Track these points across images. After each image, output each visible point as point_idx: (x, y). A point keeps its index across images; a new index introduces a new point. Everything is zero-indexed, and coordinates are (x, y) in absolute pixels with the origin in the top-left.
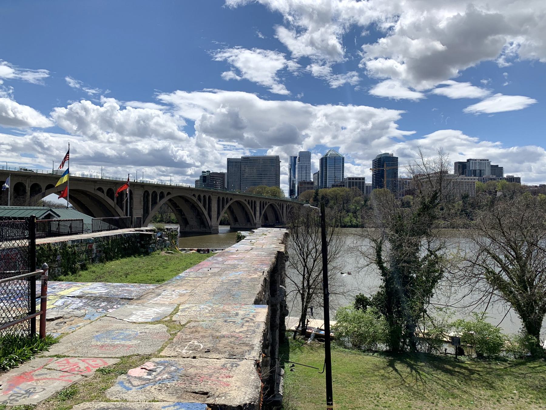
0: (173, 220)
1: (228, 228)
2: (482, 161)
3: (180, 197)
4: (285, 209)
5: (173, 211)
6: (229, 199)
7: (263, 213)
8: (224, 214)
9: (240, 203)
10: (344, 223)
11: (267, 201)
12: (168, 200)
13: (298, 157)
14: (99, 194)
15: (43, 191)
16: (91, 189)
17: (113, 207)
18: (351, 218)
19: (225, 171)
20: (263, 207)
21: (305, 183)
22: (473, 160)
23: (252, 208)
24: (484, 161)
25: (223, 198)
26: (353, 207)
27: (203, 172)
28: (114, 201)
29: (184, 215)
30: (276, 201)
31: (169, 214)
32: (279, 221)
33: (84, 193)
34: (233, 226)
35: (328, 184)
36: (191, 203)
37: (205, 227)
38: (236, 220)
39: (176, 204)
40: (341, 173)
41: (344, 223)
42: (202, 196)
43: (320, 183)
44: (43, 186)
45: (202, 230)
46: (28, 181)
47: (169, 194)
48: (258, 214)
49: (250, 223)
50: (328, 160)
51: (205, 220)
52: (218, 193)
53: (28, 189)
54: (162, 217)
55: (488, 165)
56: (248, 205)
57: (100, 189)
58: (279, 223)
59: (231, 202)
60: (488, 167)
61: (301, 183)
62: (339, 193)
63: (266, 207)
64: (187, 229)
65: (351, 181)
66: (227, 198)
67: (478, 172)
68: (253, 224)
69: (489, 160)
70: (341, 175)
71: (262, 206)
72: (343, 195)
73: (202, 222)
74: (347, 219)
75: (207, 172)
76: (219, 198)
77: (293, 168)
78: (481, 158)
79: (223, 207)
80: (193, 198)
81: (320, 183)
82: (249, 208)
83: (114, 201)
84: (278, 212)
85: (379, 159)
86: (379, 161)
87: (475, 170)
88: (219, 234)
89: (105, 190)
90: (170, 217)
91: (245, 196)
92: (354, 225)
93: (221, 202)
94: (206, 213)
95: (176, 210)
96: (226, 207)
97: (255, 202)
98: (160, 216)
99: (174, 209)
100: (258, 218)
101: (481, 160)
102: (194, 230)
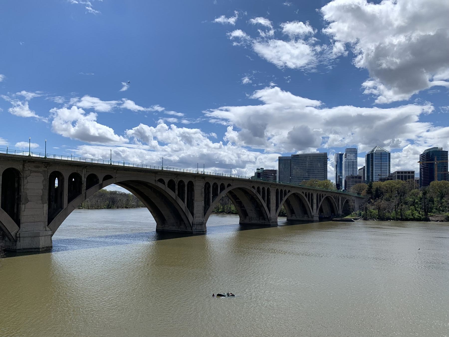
0: (233, 211)
1: (284, 220)
3: (239, 188)
4: (340, 201)
5: (233, 203)
6: (287, 191)
7: (319, 206)
8: (282, 207)
9: (297, 196)
10: (405, 216)
11: (324, 193)
12: (228, 192)
13: (345, 154)
14: (160, 185)
15: (101, 182)
16: (151, 180)
17: (175, 198)
18: (413, 211)
19: (277, 168)
20: (320, 200)
21: (353, 177)
23: (309, 200)
25: (281, 190)
26: (411, 200)
28: (175, 193)
31: (229, 205)
32: (334, 214)
33: (145, 184)
34: (290, 218)
37: (264, 219)
38: (292, 212)
39: (236, 196)
41: (405, 216)
42: (261, 188)
43: (366, 178)
44: (101, 177)
45: (261, 222)
46: (84, 171)
47: (229, 185)
48: (315, 207)
51: (264, 212)
52: (277, 185)
53: (84, 180)
54: (223, 208)
57: (161, 181)
58: (334, 215)
59: (289, 194)
62: (394, 186)
63: (322, 200)
64: (247, 221)
65: (404, 174)
66: (285, 191)
68: (310, 217)
71: (319, 199)
72: (399, 188)
73: (261, 214)
74: (408, 212)
75: (261, 169)
76: (277, 190)
77: (339, 164)
79: (281, 199)
80: (253, 190)
82: (307, 200)
83: (175, 192)
84: (334, 205)
85: (427, 153)
88: (278, 227)
89: (166, 181)
90: (230, 208)
91: (303, 188)
92: (417, 218)
93: (280, 194)
94: (265, 205)
95: (236, 202)
96: (285, 199)
97: (312, 194)
98: (222, 207)
99: (234, 201)
100: (315, 211)
102: (253, 222)
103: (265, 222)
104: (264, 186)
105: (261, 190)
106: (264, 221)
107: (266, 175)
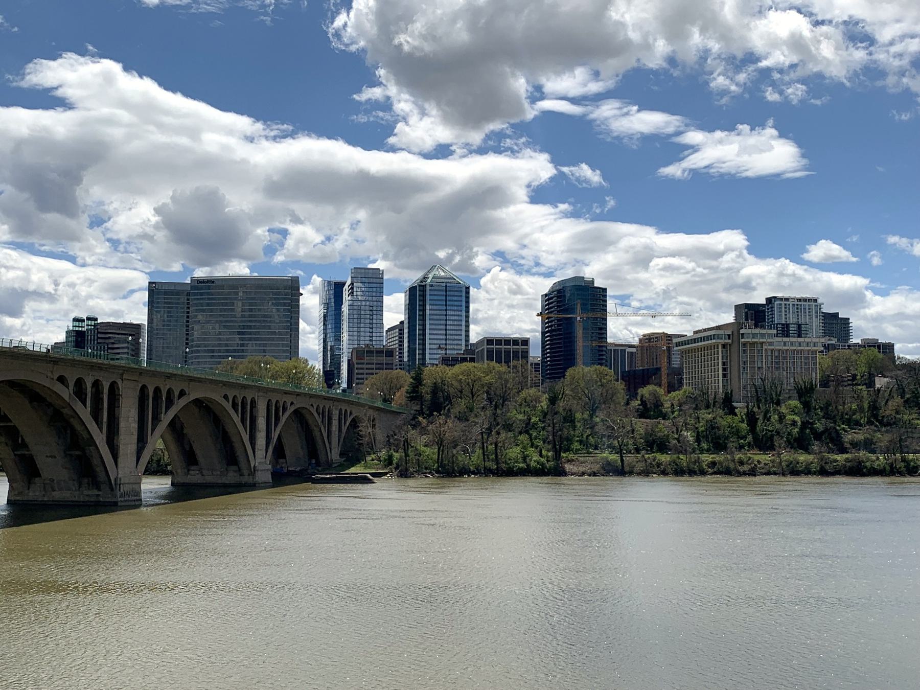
2: (802, 303)
4: (335, 423)
6: (177, 393)
7: (275, 436)
8: (157, 443)
18: (524, 447)
19: (138, 315)
21: (370, 352)
22: (781, 299)
23: (243, 421)
24: (807, 303)
25: (157, 390)
26: (520, 417)
27: (75, 320)
29: (24, 445)
30: (313, 400)
32: (317, 458)
34: (181, 479)
35: (427, 356)
36: (50, 405)
37: (96, 484)
38: (190, 459)
40: (463, 328)
41: (506, 463)
43: (406, 354)
45: (89, 494)
48: (261, 440)
49: (235, 468)
50: (428, 293)
52: (142, 372)
55: (816, 312)
56: (232, 412)
58: (318, 464)
59: (183, 402)
60: (816, 317)
61: (359, 354)
63: (283, 419)
64: (35, 494)
66: (169, 392)
67: (793, 328)
68: (246, 472)
69: (819, 301)
70: (463, 333)
74: (514, 452)
75: (88, 319)
76: (144, 389)
77: (332, 313)
78: (798, 296)
79: (156, 419)
80: (59, 388)
81: (406, 354)
82: (237, 419)
85: (559, 291)
86: (558, 297)
87: (787, 325)
91: (225, 384)
92: (535, 468)
94: (100, 439)
96: (167, 418)
97: (253, 402)
100: (260, 453)
101: (799, 300)
102: (57, 495)
103: (98, 495)
104: (100, 376)
105: (89, 389)
106: (96, 492)
107: (107, 341)
